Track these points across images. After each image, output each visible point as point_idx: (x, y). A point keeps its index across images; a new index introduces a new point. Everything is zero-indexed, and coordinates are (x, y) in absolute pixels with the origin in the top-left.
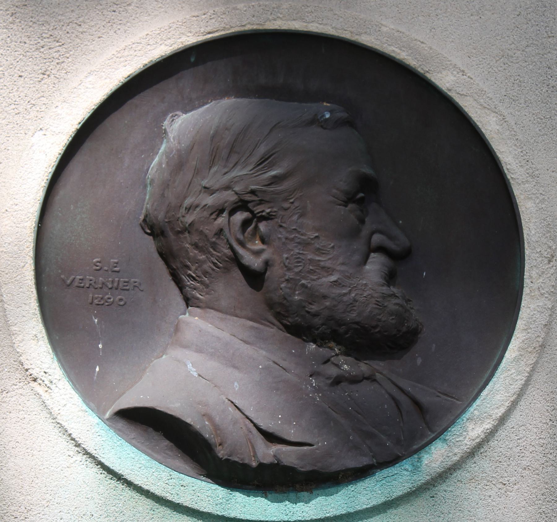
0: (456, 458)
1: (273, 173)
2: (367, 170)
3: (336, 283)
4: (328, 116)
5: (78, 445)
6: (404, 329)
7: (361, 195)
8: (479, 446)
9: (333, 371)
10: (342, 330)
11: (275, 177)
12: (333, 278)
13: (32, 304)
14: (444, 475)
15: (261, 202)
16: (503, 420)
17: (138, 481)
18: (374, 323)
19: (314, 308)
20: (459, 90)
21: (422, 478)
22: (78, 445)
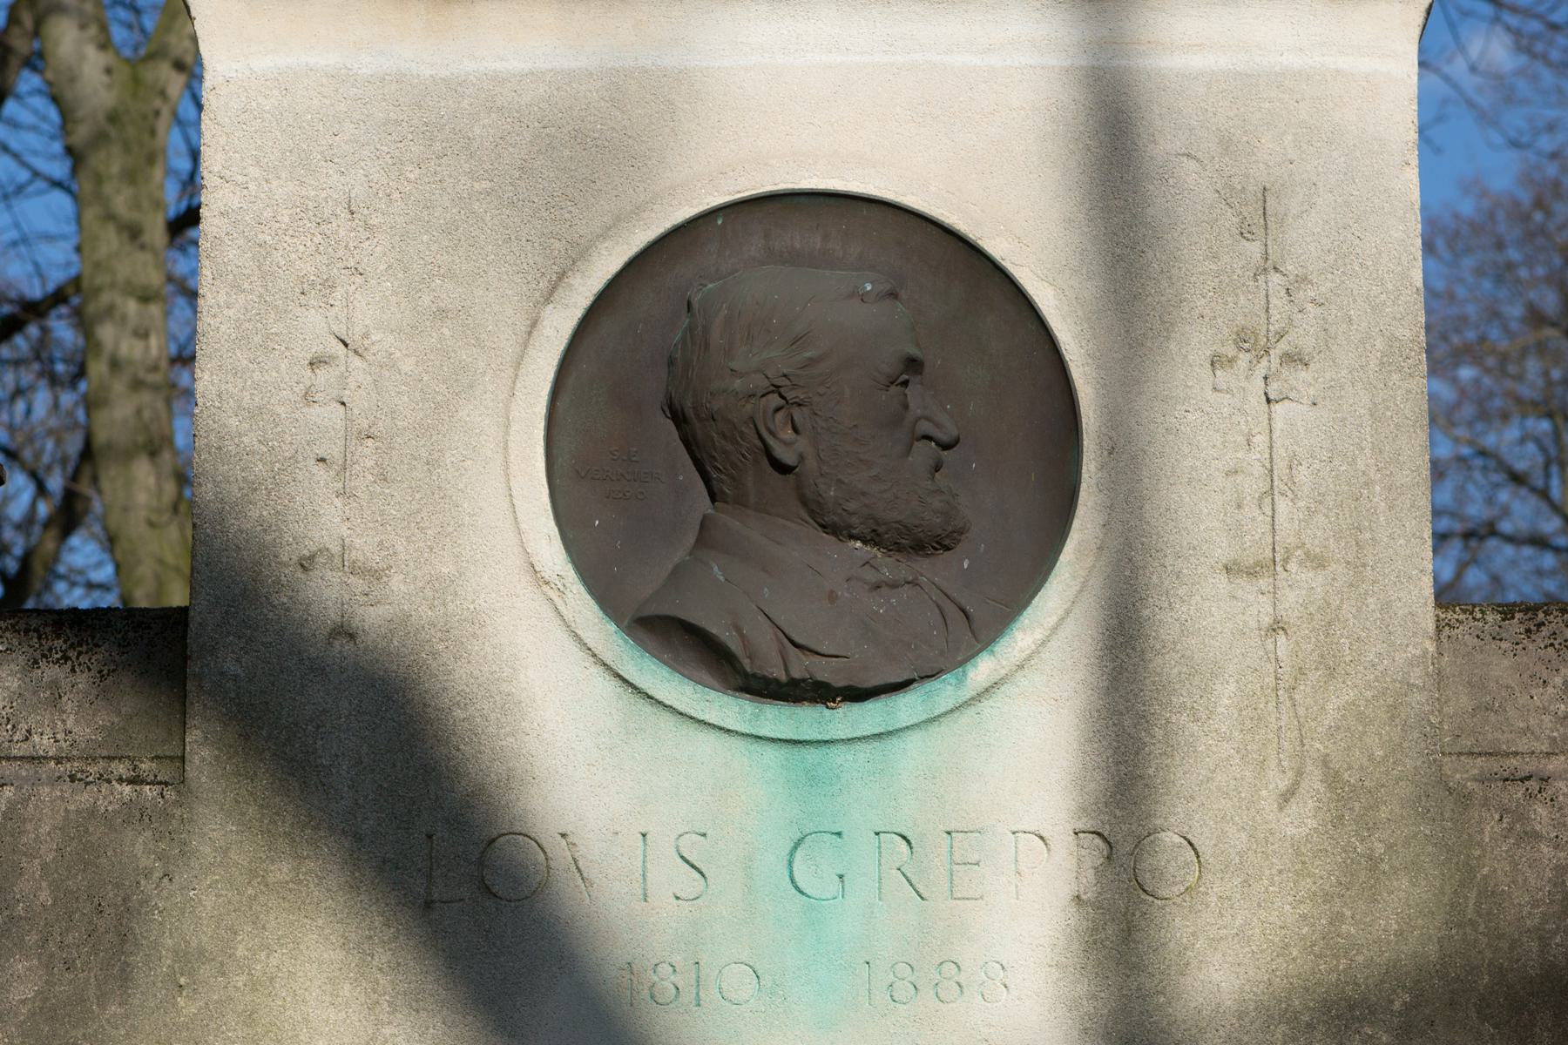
0: (1003, 672)
1: (808, 354)
2: (914, 351)
3: (876, 478)
4: (869, 288)
5: (594, 655)
6: (950, 529)
7: (905, 377)
8: (1029, 658)
9: (870, 576)
10: (881, 530)
11: (810, 359)
12: (873, 473)
13: (220, 156)
14: (987, 692)
15: (794, 386)
16: (1271, 447)
17: (681, 708)
18: (917, 522)
19: (852, 506)
20: (1014, 259)
21: (966, 693)
22: (594, 655)
